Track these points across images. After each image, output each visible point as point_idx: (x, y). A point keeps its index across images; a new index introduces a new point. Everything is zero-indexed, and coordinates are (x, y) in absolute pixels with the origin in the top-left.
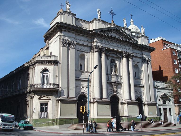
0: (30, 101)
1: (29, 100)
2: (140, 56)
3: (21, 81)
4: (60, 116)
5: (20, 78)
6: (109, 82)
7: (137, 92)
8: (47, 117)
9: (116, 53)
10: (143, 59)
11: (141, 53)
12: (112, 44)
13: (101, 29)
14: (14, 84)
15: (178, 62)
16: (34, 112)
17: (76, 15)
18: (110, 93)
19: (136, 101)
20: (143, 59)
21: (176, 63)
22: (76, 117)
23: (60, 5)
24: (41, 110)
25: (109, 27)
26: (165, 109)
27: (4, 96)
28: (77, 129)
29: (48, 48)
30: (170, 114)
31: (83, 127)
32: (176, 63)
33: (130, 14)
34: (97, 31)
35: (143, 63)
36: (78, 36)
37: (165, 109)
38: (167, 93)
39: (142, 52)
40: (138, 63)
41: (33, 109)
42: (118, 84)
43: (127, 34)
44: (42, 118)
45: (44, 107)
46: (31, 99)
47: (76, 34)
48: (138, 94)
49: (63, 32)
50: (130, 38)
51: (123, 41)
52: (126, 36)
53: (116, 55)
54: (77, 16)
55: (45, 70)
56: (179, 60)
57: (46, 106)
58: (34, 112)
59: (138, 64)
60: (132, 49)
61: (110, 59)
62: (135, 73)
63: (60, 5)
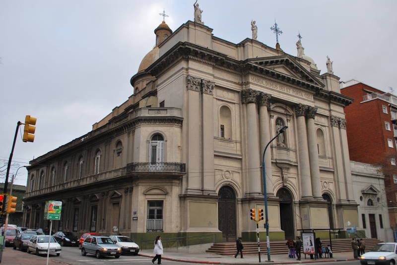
0: (124, 196)
1: (122, 195)
2: (327, 113)
3: (99, 156)
4: (49, 235)
5: (98, 151)
6: (275, 161)
7: (323, 182)
8: (162, 230)
9: (284, 106)
10: (331, 119)
11: (327, 108)
12: (278, 89)
13: (261, 60)
14: (81, 162)
15: (391, 127)
16: (134, 219)
17: (213, 30)
19: (323, 200)
20: (331, 119)
21: (389, 129)
22: (216, 230)
23: (160, 14)
24: (151, 216)
25: (272, 56)
26: (372, 216)
27: (58, 187)
28: (230, 254)
29: (154, 93)
30: (382, 226)
31: (259, 248)
32: (389, 129)
33: (298, 35)
35: (332, 126)
36: (218, 71)
37: (372, 216)
38: (374, 185)
39: (330, 106)
41: (132, 214)
43: (305, 70)
44: (151, 231)
45: (156, 208)
46: (126, 192)
47: (214, 67)
49: (190, 62)
50: (310, 78)
51: (298, 83)
52: (304, 75)
53: (285, 109)
54: (216, 34)
55: (158, 137)
56: (394, 122)
57: (159, 208)
58: (134, 219)
59: (323, 128)
60: (313, 100)
61: (276, 116)
63: (160, 14)
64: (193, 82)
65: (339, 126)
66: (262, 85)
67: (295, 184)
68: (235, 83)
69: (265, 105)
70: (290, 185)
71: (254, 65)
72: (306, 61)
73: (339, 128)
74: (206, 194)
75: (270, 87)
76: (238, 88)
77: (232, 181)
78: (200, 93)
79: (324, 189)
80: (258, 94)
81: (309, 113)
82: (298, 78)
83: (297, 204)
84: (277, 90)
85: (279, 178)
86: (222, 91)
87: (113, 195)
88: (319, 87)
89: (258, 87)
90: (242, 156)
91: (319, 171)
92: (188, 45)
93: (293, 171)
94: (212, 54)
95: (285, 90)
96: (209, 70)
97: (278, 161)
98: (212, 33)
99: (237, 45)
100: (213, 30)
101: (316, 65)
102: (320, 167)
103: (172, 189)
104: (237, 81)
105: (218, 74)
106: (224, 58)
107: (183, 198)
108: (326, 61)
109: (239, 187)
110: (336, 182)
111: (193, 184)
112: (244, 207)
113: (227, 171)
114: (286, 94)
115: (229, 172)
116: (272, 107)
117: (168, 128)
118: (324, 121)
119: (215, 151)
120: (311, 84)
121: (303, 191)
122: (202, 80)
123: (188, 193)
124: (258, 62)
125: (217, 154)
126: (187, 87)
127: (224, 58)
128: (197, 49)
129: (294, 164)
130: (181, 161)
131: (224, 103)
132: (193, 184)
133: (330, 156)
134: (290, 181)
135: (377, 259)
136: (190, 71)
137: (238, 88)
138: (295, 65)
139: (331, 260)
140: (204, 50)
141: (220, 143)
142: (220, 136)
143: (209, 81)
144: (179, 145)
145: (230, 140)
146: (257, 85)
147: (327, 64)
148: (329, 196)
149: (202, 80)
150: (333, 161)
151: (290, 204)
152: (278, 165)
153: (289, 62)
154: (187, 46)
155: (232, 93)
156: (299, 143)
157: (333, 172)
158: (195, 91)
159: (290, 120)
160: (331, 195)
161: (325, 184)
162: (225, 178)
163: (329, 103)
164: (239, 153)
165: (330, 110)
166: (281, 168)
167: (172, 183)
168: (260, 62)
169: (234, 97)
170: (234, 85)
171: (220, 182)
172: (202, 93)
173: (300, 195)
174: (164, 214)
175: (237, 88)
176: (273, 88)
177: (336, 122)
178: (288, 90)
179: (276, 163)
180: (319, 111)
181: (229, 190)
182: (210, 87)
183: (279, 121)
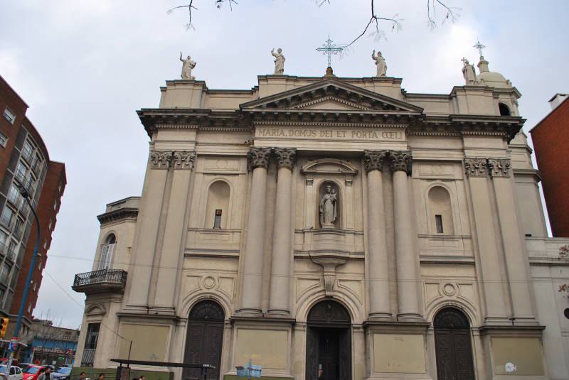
2: (457, 156)
7: (442, 285)
9: (337, 161)
11: (459, 146)
17: (401, 79)
18: (309, 293)
25: (293, 88)
39: (463, 142)
40: (447, 184)
42: (342, 262)
48: (446, 294)
49: (465, 139)
51: (372, 118)
61: (318, 181)
65: (490, 174)
67: (358, 293)
68: (237, 145)
71: (254, 110)
72: (363, 79)
73: (492, 178)
74: (153, 313)
76: (244, 151)
77: (219, 294)
78: (489, 177)
79: (446, 298)
81: (389, 163)
82: (366, 110)
84: (316, 137)
85: (317, 282)
86: (216, 161)
88: (410, 113)
90: (474, 258)
92: (147, 112)
93: (351, 270)
94: (496, 121)
95: (308, 134)
96: (191, 136)
97: (312, 255)
98: (402, 86)
99: (450, 95)
100: (401, 79)
101: (508, 81)
104: (242, 142)
105: (204, 138)
106: (518, 122)
107: (121, 316)
108: (462, 66)
109: (472, 309)
110: (480, 282)
111: (136, 298)
112: (369, 337)
113: (209, 277)
114: (337, 141)
115: (452, 285)
116: (306, 167)
117: (121, 225)
118: (455, 172)
119: (421, 256)
121: (371, 304)
122: (173, 153)
123: (488, 324)
124: (264, 104)
125: (533, 261)
127: (518, 122)
128: (160, 114)
129: (353, 256)
130: (379, 71)
131: (218, 176)
132: (136, 298)
133: (466, 233)
134: (343, 287)
136: (466, 151)
137: (244, 151)
138: (349, 91)
140: (172, 112)
141: (202, 236)
142: (435, 233)
143: (476, 159)
145: (451, 238)
146: (266, 139)
147: (464, 72)
148: (461, 312)
149: (487, 160)
150: (472, 243)
151: (347, 329)
152: (316, 261)
153: (332, 87)
155: (450, 165)
156: (368, 216)
157: (473, 264)
158: (479, 176)
159: (351, 183)
160: (466, 310)
161: (449, 289)
164: (470, 255)
165: (463, 150)
166: (321, 265)
167: (110, 298)
168: (267, 104)
169: (241, 166)
170: (238, 148)
171: (193, 295)
172: (492, 178)
173: (481, 315)
174: (100, 342)
176: (307, 137)
179: (310, 258)
180: (416, 155)
181: (456, 314)
183: (326, 188)
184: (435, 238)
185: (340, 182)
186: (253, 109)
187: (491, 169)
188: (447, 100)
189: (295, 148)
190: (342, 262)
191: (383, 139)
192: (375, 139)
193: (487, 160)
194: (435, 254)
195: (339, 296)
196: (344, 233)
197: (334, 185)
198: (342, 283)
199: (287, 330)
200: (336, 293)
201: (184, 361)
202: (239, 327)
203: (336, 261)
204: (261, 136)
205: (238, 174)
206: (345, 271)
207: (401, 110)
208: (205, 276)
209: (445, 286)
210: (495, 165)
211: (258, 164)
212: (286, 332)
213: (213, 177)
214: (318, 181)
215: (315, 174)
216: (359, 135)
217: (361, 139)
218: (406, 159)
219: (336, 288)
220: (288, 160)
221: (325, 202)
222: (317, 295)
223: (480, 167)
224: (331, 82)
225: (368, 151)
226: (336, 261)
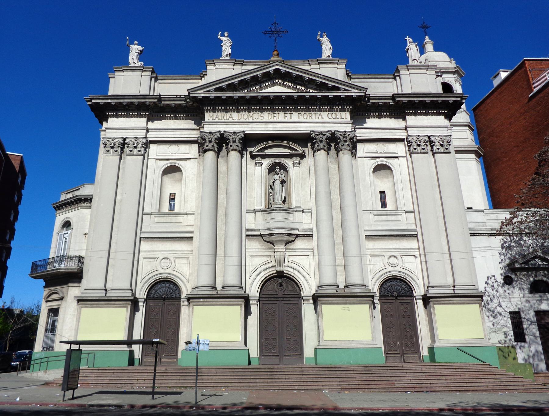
2: (401, 134)
7: (386, 258)
9: (285, 143)
18: (264, 267)
34: (199, 92)
40: (390, 161)
42: (292, 238)
49: (407, 117)
61: (267, 162)
62: (284, 303)
64: (416, 142)
66: (230, 120)
69: (233, 150)
70: (294, 269)
71: (203, 95)
75: (247, 120)
79: (390, 269)
80: (328, 135)
82: (312, 92)
83: (308, 300)
84: (264, 120)
87: (48, 297)
88: (354, 93)
89: (217, 126)
91: (196, 236)
100: (175, 194)
102: (366, 231)
103: (68, 290)
113: (165, 258)
116: (255, 150)
119: (470, 229)
120: (331, 94)
122: (429, 137)
123: (430, 292)
125: (473, 232)
126: (432, 151)
128: (109, 101)
131: (170, 161)
135: (38, 407)
139: (173, 211)
142: (379, 208)
144: (87, 231)
145: (395, 212)
149: (429, 137)
152: (267, 239)
154: (93, 101)
158: (421, 153)
160: (409, 279)
161: (393, 260)
162: (387, 266)
163: (404, 119)
168: (215, 89)
169: (194, 149)
172: (218, 157)
175: (194, 136)
176: (255, 120)
177: (419, 145)
178: (334, 116)
179: (261, 236)
182: (445, 143)
184: (379, 213)
185: (288, 162)
186: (201, 94)
187: (433, 145)
188: (391, 80)
189: (244, 132)
190: (292, 238)
191: (328, 120)
192: (320, 120)
193: (125, 139)
194: (380, 228)
195: (288, 271)
196: (293, 211)
197: (284, 168)
198: (292, 258)
199: (240, 305)
200: (286, 268)
201: (128, 338)
202: (194, 304)
203: (285, 238)
204: (211, 120)
205: (189, 159)
206: (294, 247)
207: (346, 90)
208: (161, 258)
209: (389, 257)
210: (436, 141)
211: (208, 148)
212: (239, 307)
213: (165, 162)
214: (267, 162)
215: (264, 156)
216: (305, 117)
217: (307, 120)
218: (351, 138)
219: (286, 263)
220: (324, 143)
221: (274, 182)
222: (268, 270)
223: (422, 144)
224: (277, 65)
225: (314, 132)
226: (285, 238)
